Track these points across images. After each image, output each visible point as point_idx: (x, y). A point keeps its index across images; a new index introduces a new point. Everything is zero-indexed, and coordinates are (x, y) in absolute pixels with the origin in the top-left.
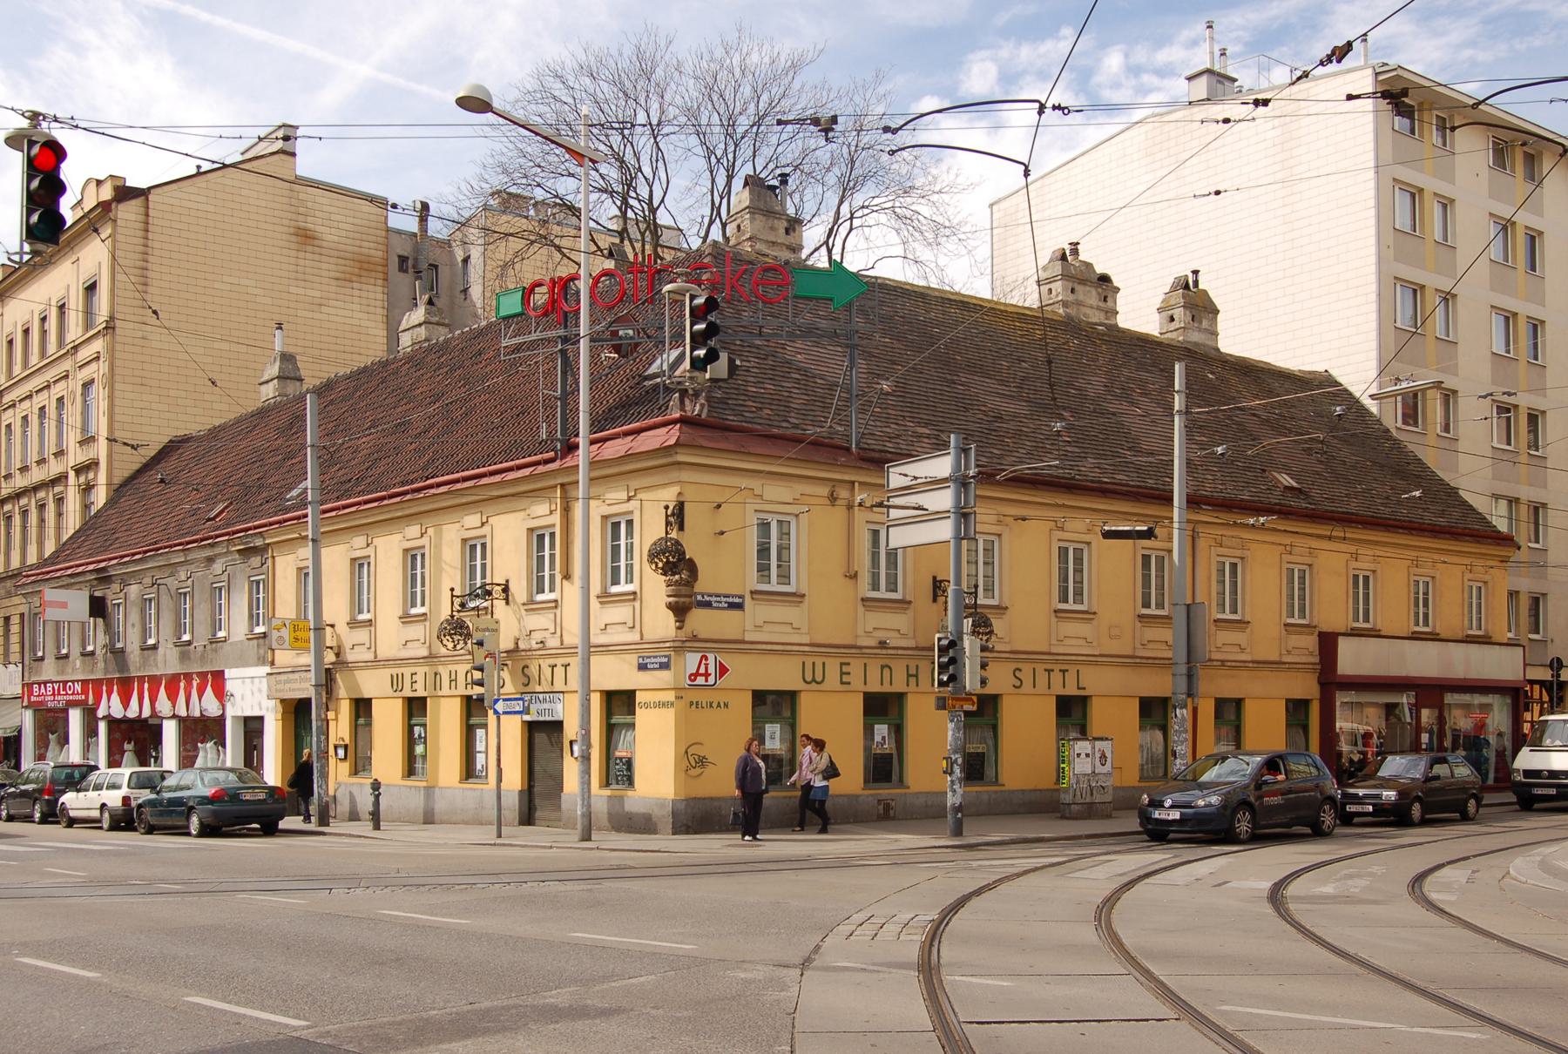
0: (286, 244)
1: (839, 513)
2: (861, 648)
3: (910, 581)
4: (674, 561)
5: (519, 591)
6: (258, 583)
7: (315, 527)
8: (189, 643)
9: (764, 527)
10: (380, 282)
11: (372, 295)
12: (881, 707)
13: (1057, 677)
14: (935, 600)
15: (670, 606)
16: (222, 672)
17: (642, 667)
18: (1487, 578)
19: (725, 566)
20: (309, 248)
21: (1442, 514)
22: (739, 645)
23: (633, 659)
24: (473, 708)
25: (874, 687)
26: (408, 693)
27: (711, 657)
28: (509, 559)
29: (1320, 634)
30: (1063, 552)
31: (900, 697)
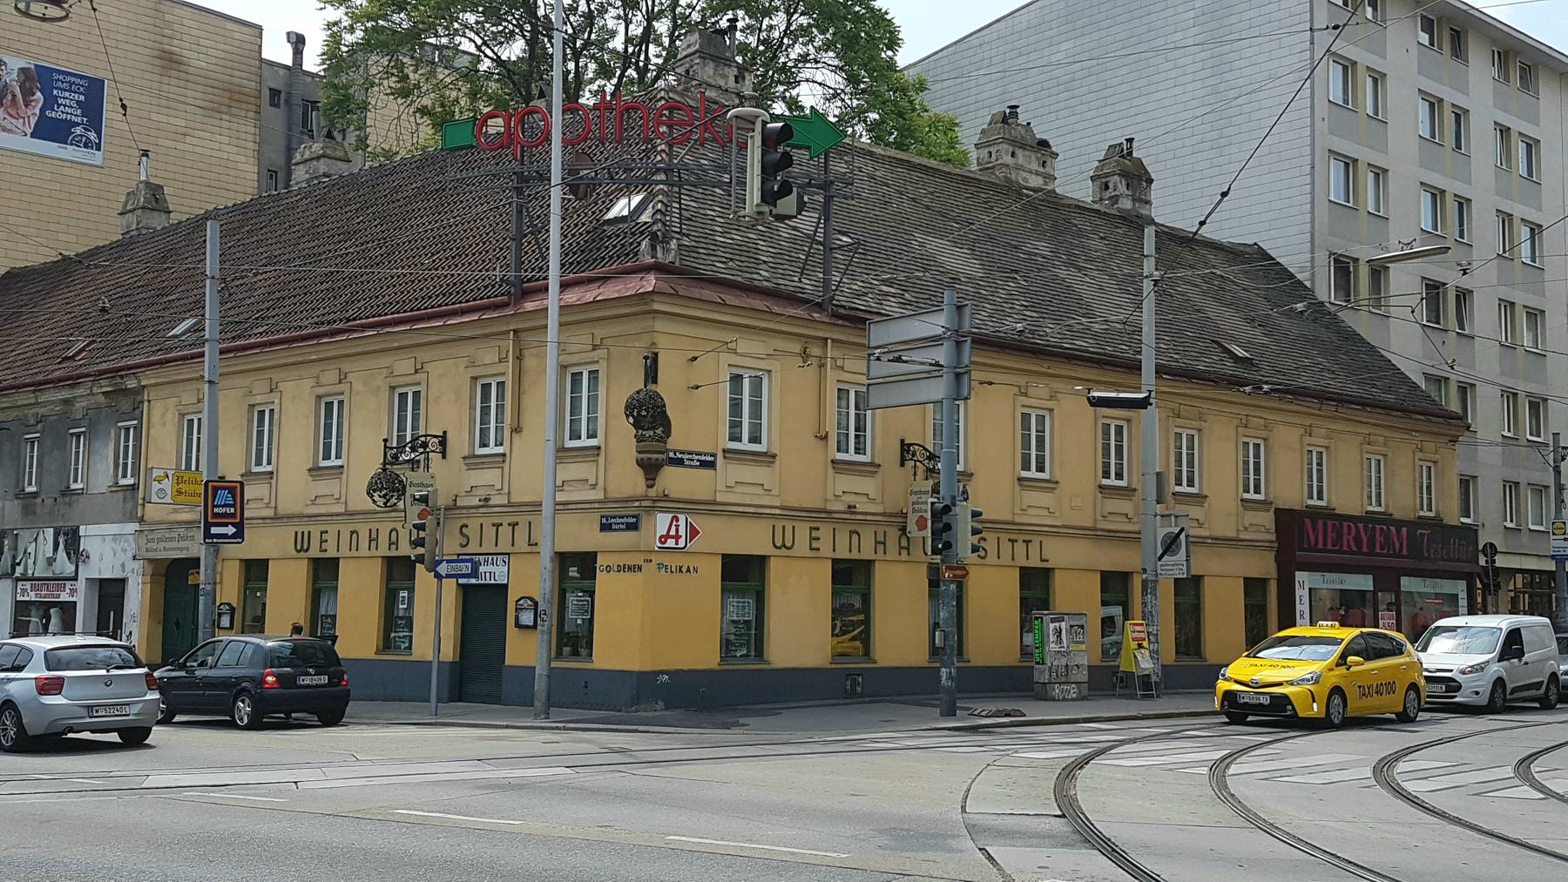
0: (149, 67)
1: (811, 372)
2: (830, 512)
3: (878, 442)
4: (649, 415)
5: (459, 444)
6: (127, 429)
7: (213, 367)
8: (35, 495)
9: (736, 380)
10: (251, 114)
11: (242, 128)
12: (851, 578)
13: (1020, 548)
14: (902, 465)
15: (640, 463)
16: (76, 531)
17: (605, 528)
18: (1437, 457)
19: (696, 423)
20: (174, 73)
21: (1388, 391)
22: (709, 507)
23: (594, 521)
24: (398, 572)
25: (842, 553)
26: (315, 552)
27: (682, 518)
28: (448, 411)
29: (1277, 510)
30: (1026, 418)
31: (868, 565)
